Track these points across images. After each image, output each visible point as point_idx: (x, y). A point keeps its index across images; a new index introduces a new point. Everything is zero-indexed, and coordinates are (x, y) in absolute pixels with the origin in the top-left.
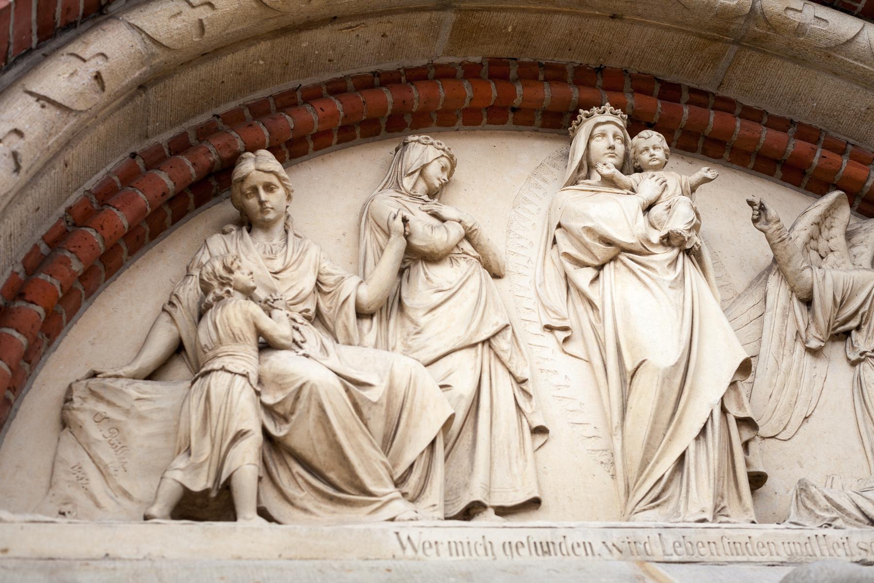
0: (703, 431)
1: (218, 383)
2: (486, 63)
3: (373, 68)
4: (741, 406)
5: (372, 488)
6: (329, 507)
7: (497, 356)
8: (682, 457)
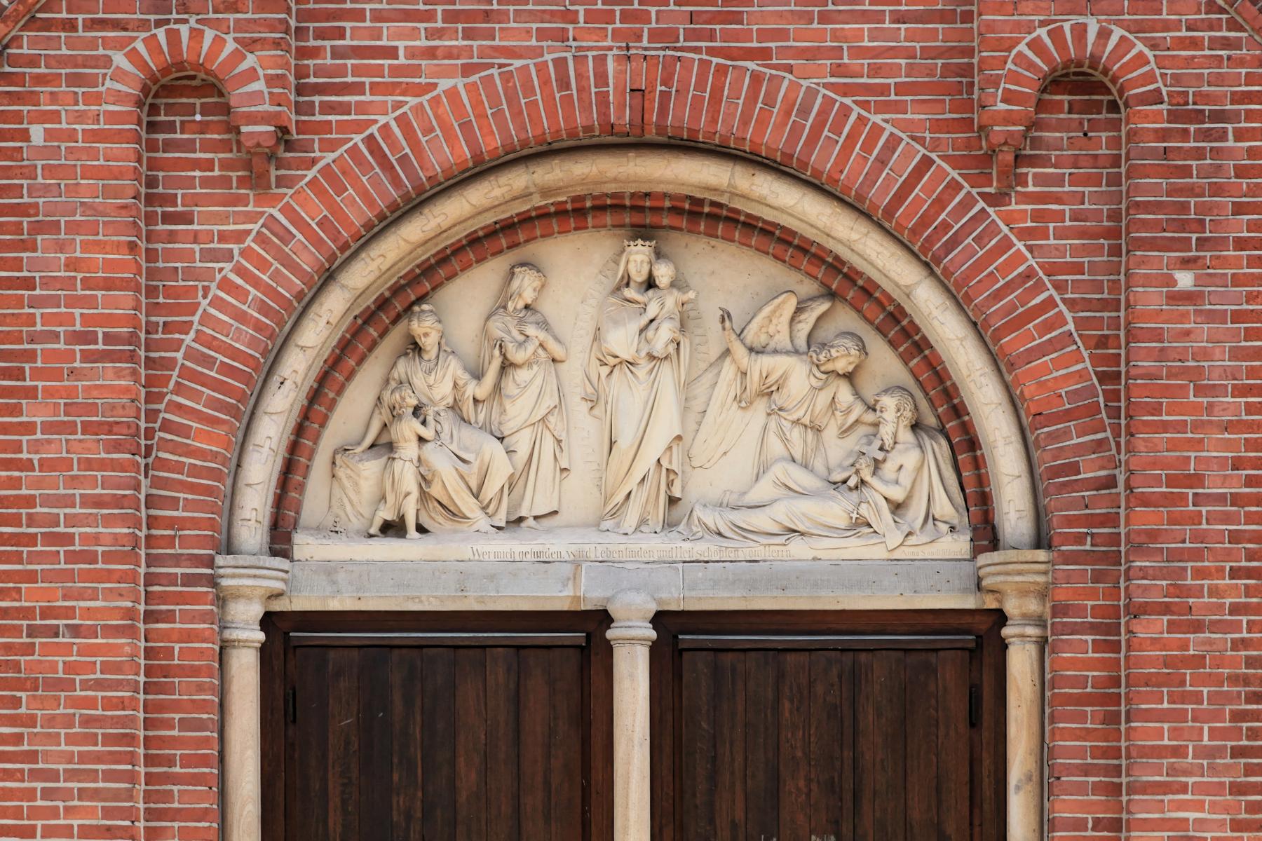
0: (643, 479)
1: (397, 465)
2: (569, 201)
3: (495, 219)
4: (670, 462)
5: (469, 515)
6: (450, 523)
7: (547, 427)
8: (630, 493)
